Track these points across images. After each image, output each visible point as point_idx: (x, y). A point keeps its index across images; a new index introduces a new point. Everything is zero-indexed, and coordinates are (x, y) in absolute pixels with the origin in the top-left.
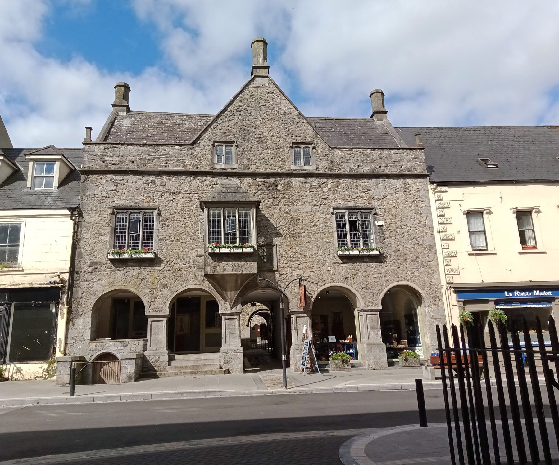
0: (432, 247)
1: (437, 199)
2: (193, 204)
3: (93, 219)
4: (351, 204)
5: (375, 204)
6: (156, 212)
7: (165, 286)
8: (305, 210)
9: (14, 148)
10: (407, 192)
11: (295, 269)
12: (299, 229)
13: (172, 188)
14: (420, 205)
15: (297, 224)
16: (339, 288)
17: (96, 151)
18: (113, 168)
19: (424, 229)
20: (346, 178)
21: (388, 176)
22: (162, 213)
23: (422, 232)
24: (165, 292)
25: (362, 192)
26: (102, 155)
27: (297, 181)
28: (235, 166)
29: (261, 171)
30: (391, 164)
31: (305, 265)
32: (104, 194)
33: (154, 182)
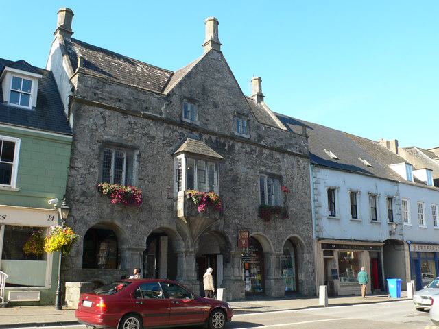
4: (269, 171)
27: (238, 146)
31: (240, 216)
32: (94, 127)
33: (136, 124)
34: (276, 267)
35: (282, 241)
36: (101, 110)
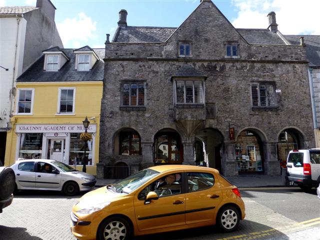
0: (310, 106)
1: (313, 77)
2: (167, 79)
3: (111, 87)
4: (261, 79)
5: (276, 79)
6: (145, 83)
7: (151, 126)
8: (234, 83)
9: (65, 48)
10: (295, 73)
11: (227, 118)
12: (229, 94)
13: (155, 69)
14: (303, 80)
15: (229, 91)
16: (167, 130)
17: (112, 48)
18: (122, 57)
19: (305, 95)
20: (112, 59)
21: (284, 62)
22: (150, 84)
23: (303, 97)
24: (151, 129)
25: (267, 72)
26: (116, 50)
28: (191, 56)
29: (207, 59)
30: (286, 56)
31: (232, 116)
32: (117, 73)
33: (144, 66)
34: (272, 153)
35: (277, 132)
36: (121, 62)
